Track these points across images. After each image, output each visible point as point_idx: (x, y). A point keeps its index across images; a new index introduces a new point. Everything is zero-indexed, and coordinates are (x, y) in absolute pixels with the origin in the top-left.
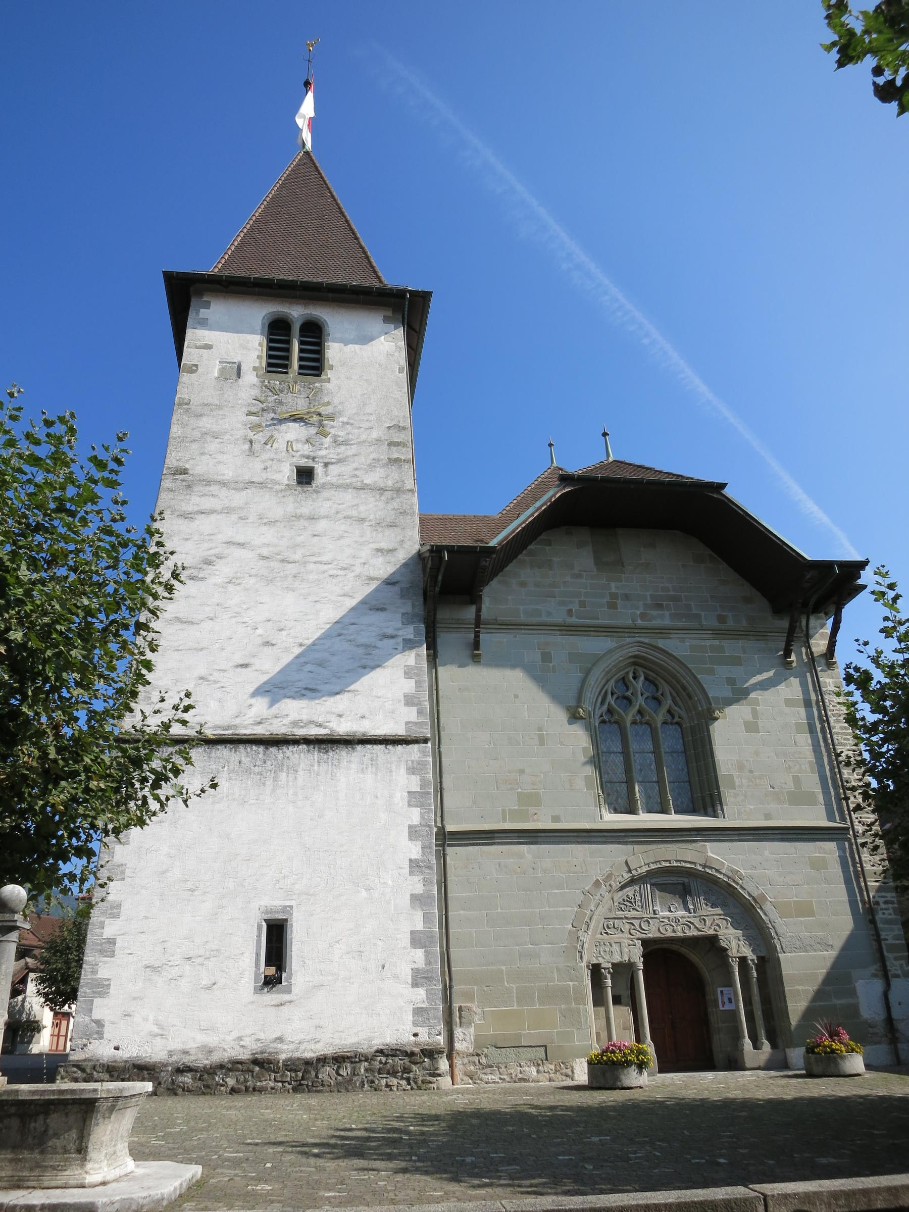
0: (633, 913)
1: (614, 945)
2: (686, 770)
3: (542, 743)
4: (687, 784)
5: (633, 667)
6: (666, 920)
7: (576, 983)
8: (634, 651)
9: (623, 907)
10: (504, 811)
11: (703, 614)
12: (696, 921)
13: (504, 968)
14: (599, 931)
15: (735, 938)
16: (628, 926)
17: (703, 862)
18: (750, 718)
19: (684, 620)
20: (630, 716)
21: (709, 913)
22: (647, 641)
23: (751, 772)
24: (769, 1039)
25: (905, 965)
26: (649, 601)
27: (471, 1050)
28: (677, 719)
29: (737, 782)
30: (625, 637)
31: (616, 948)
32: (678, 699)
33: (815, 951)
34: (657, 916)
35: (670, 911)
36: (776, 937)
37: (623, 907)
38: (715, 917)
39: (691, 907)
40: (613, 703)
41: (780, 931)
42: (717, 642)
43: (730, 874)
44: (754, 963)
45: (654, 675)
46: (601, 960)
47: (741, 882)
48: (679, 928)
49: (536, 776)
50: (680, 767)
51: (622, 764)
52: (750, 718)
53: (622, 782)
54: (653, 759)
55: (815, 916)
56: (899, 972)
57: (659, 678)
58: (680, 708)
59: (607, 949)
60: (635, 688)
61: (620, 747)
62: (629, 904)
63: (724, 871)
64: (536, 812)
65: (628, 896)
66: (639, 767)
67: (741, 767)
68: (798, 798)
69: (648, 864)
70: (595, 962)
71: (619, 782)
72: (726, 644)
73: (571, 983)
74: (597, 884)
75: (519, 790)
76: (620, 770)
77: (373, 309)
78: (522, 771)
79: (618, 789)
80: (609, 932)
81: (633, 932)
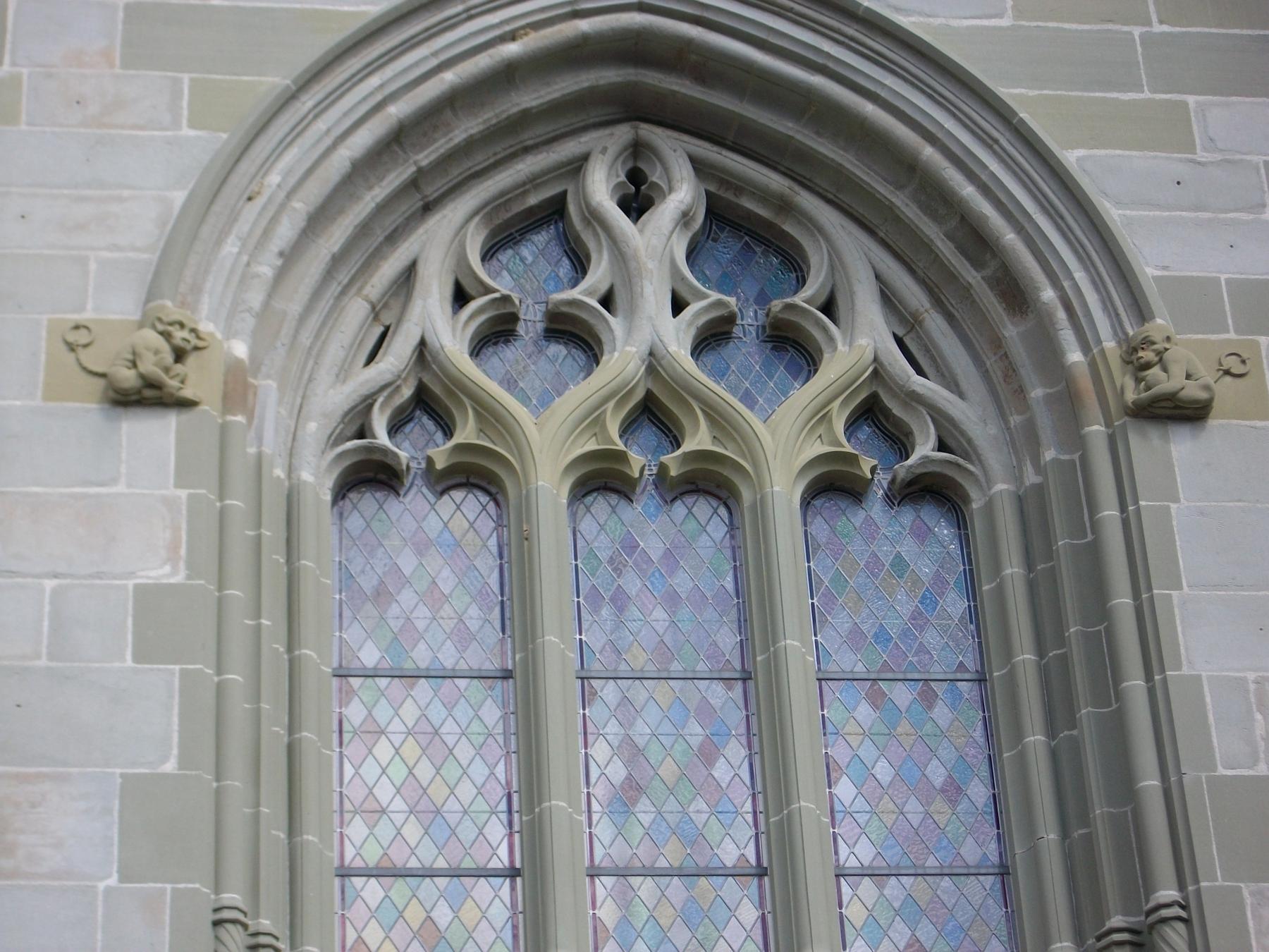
2: (979, 792)
4: (982, 889)
5: (623, 133)
11: (1242, 885)
32: (935, 323)
45: (775, 181)
50: (937, 774)
51: (495, 751)
53: (483, 873)
54: (736, 718)
57: (807, 201)
58: (953, 386)
60: (621, 256)
61: (492, 635)
66: (618, 772)
68: (423, 426)
71: (455, 873)
76: (466, 791)
77: (636, 26)
79: (443, 915)
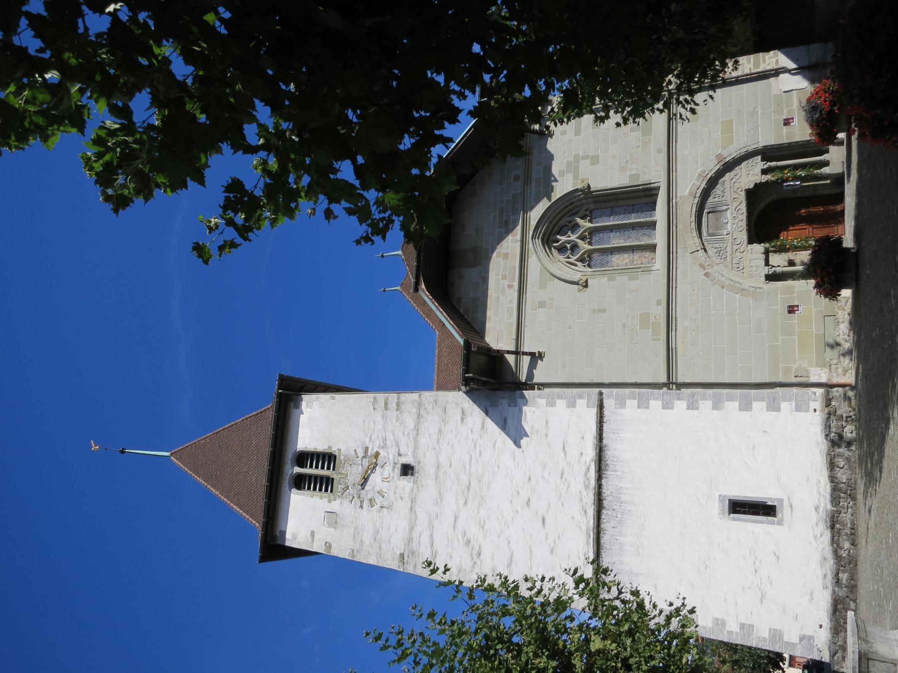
0: (729, 249)
1: (752, 264)
3: (604, 310)
6: (734, 226)
7: (779, 293)
8: (538, 242)
9: (723, 257)
10: (653, 340)
12: (735, 204)
13: (767, 344)
14: (741, 275)
15: (747, 177)
16: (738, 254)
17: (692, 198)
18: (588, 161)
19: (517, 205)
20: (584, 246)
21: (729, 195)
22: (531, 233)
23: (627, 162)
24: (820, 168)
25: (769, 56)
26: (503, 230)
27: (827, 370)
28: (588, 213)
29: (634, 172)
30: (528, 248)
31: (754, 263)
33: (758, 120)
34: (731, 232)
35: (727, 223)
36: (747, 148)
37: (723, 257)
38: (732, 190)
39: (725, 208)
40: (575, 258)
41: (743, 145)
42: (533, 183)
43: (701, 179)
44: (766, 164)
46: (763, 274)
47: (707, 172)
48: (740, 217)
49: (628, 315)
52: (588, 161)
55: (733, 120)
56: (774, 60)
59: (754, 269)
62: (722, 252)
63: (699, 184)
64: (653, 317)
65: (716, 253)
67: (623, 169)
69: (693, 237)
70: (764, 278)
72: (534, 177)
73: (779, 296)
74: (707, 275)
75: (638, 328)
78: (624, 325)
80: (742, 267)
81: (742, 250)
